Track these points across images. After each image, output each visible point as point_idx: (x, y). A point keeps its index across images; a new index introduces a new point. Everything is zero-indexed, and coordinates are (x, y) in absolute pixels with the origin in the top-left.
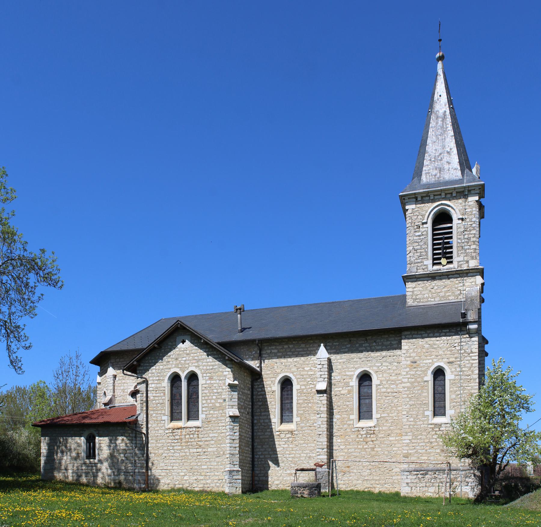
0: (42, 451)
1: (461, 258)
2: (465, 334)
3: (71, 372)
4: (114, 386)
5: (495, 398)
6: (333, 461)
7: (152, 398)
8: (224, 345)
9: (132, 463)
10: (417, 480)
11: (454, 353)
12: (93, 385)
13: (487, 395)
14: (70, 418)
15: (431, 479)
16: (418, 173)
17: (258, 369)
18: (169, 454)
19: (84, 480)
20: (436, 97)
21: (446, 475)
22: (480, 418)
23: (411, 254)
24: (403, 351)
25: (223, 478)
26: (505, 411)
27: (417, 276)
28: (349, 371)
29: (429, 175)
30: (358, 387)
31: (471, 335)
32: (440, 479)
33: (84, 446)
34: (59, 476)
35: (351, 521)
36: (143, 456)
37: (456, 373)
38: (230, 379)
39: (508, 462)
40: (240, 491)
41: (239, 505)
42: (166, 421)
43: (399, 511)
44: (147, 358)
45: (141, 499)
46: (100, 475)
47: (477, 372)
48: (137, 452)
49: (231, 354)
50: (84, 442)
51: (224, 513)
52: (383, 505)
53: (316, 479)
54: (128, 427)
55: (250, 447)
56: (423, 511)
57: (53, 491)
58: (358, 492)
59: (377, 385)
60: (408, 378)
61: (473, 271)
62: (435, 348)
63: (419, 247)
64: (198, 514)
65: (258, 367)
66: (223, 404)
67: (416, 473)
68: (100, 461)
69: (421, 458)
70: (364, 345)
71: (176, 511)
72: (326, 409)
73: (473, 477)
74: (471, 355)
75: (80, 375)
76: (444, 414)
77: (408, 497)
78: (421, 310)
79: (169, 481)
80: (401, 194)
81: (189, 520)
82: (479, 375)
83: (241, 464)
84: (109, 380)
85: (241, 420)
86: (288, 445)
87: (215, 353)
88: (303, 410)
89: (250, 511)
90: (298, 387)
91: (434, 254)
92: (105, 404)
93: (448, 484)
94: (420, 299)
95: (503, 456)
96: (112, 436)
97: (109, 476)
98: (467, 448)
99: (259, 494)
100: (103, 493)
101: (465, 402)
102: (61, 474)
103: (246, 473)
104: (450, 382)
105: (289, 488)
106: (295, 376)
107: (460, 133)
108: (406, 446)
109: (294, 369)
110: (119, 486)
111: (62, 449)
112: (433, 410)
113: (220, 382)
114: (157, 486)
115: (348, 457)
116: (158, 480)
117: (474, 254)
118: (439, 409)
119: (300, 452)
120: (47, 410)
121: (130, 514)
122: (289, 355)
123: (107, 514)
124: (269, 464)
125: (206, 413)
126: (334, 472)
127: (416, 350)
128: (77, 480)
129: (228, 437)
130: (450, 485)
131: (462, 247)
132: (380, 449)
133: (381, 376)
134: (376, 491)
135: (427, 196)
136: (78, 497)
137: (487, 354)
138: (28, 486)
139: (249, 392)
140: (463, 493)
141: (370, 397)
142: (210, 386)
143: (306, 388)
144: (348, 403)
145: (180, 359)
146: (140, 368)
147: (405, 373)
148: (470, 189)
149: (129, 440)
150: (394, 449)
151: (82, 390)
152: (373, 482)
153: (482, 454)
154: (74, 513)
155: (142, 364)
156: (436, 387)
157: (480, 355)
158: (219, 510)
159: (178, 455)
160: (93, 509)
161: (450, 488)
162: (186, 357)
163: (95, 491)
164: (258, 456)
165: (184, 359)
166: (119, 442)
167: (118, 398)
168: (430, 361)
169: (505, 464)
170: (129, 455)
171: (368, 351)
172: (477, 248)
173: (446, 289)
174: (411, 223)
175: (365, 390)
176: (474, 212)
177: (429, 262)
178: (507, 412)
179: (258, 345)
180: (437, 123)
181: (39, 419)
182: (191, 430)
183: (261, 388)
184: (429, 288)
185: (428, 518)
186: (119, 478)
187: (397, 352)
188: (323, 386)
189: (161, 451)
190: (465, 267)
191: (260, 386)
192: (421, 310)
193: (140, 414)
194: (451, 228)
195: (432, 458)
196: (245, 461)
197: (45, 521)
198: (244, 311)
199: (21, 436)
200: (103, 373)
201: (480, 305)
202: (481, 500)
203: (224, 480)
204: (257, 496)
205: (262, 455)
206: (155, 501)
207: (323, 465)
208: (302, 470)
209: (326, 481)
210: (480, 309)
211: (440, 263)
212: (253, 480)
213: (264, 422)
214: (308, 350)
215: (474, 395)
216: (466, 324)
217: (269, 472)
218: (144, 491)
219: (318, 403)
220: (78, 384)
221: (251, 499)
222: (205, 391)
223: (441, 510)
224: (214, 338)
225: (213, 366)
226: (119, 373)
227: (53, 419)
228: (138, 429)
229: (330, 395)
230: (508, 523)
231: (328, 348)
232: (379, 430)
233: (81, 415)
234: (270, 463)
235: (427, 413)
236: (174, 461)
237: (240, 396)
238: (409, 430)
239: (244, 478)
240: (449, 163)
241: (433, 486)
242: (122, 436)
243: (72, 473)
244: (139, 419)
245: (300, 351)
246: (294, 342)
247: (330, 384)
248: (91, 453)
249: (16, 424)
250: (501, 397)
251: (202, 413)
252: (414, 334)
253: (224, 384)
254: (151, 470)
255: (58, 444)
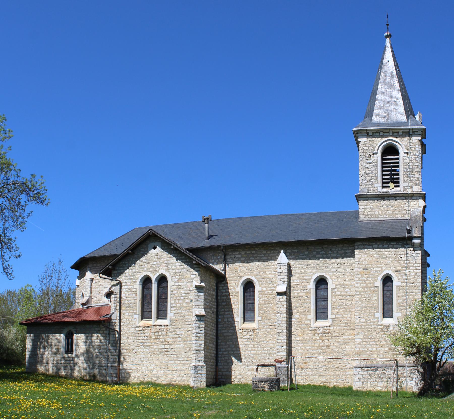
0: (27, 347)
1: (406, 184)
2: (410, 247)
3: (54, 276)
4: (91, 288)
5: (436, 303)
6: (291, 357)
7: (125, 298)
8: (193, 251)
9: (105, 358)
10: (368, 376)
11: (401, 263)
12: (72, 288)
13: (428, 301)
14: (51, 317)
15: (381, 375)
16: (370, 114)
17: (223, 272)
18: (139, 350)
19: (62, 372)
20: (385, 62)
21: (393, 371)
22: (423, 321)
23: (363, 178)
24: (356, 259)
25: (188, 372)
26: (444, 315)
27: (368, 196)
28: (307, 276)
29: (379, 116)
30: (315, 290)
31: (415, 249)
32: (388, 375)
33: (63, 342)
34: (41, 369)
35: (308, 413)
36: (116, 352)
37: (402, 280)
38: (197, 282)
39: (447, 360)
40: (205, 385)
41: (204, 398)
42: (137, 319)
43: (352, 403)
44: (121, 263)
45: (113, 391)
46: (77, 368)
47: (420, 280)
48: (110, 348)
49: (198, 259)
50: (63, 338)
51: (189, 405)
52: (337, 398)
53: (276, 374)
54: (102, 325)
55: (215, 343)
56: (373, 404)
57: (36, 382)
58: (314, 386)
59: (332, 289)
60: (361, 283)
61: (417, 195)
62: (384, 258)
63: (370, 172)
64: (165, 405)
65: (223, 270)
66: (190, 304)
67: (367, 369)
68: (77, 356)
69: (371, 355)
70: (320, 253)
71: (144, 402)
72: (285, 309)
73: (417, 373)
74: (415, 265)
75: (61, 279)
76: (392, 317)
77: (360, 391)
78: (372, 225)
79: (139, 375)
80: (354, 129)
81: (156, 411)
82: (422, 283)
83: (206, 360)
84: (86, 283)
85: (206, 319)
86: (250, 342)
87: (183, 257)
88: (264, 310)
89: (213, 404)
90: (260, 289)
91: (383, 179)
92: (83, 305)
93: (395, 379)
94: (371, 215)
95: (443, 355)
96: (88, 333)
97: (85, 369)
98: (412, 347)
99: (222, 388)
100: (79, 385)
101: (410, 306)
102: (42, 367)
103: (211, 368)
104: (397, 288)
105: (250, 383)
106: (257, 279)
107: (405, 89)
108: (359, 344)
109: (257, 273)
110: (93, 379)
111: (44, 345)
112: (382, 312)
113: (188, 284)
114: (127, 379)
115: (306, 354)
116: (129, 373)
117: (417, 182)
118: (387, 312)
119: (261, 349)
120: (32, 310)
121: (102, 404)
122: (251, 260)
123: (82, 404)
124: (232, 360)
125: (174, 312)
126: (293, 368)
127: (367, 259)
128: (57, 373)
129: (194, 335)
130: (397, 380)
131: (407, 175)
132: (335, 347)
133: (336, 280)
134: (331, 385)
135: (377, 132)
136: (57, 388)
137: (428, 266)
138: (15, 378)
139: (214, 293)
140: (408, 388)
141: (326, 299)
142: (179, 287)
143: (267, 290)
144: (306, 305)
145: (151, 264)
146: (115, 272)
147: (357, 279)
148: (414, 130)
149: (103, 336)
150: (347, 347)
151: (63, 292)
152: (328, 377)
153: (425, 353)
154: (53, 403)
155: (117, 268)
156: (385, 292)
157: (423, 266)
158: (185, 402)
159: (148, 351)
160: (69, 399)
161: (397, 383)
162: (157, 262)
163: (71, 383)
164: (222, 353)
165: (155, 263)
166: (94, 338)
167: (94, 299)
168: (380, 269)
169: (444, 361)
170: (103, 350)
171: (324, 258)
172: (420, 177)
173: (393, 208)
174: (363, 153)
175: (321, 293)
176: (417, 149)
177: (379, 185)
178: (445, 316)
179: (223, 250)
180: (385, 80)
181: (25, 318)
182: (160, 328)
183: (225, 289)
184: (379, 207)
185: (378, 410)
186: (94, 371)
187: (351, 260)
188: (283, 288)
189: (132, 347)
190: (410, 191)
191: (225, 288)
192: (372, 225)
193: (113, 313)
194: (398, 159)
195: (381, 356)
196: (209, 357)
197: (27, 409)
198: (211, 221)
199: (10, 333)
200: (81, 277)
201: (423, 224)
202: (424, 394)
203: (189, 375)
204: (221, 389)
205: (225, 351)
206: (125, 393)
207: (283, 361)
208: (263, 365)
209: (285, 376)
210: (422, 227)
211: (389, 187)
212: (216, 375)
213: (228, 321)
214: (269, 256)
215: (418, 300)
216: (411, 238)
217: (233, 367)
218: (116, 383)
219: (278, 304)
220: (60, 287)
221: (214, 392)
222: (173, 292)
223: (389, 403)
224: (182, 244)
225: (181, 269)
226: (96, 276)
227: (37, 318)
228: (111, 327)
229: (290, 296)
230: (447, 413)
231: (288, 254)
232: (334, 330)
233: (60, 314)
234: (233, 359)
235: (377, 315)
236: (143, 356)
237: (206, 297)
238: (361, 330)
239: (208, 372)
240: (396, 110)
241: (382, 381)
242: (97, 333)
243: (52, 366)
244: (113, 317)
245: (262, 257)
246: (256, 249)
247: (289, 287)
248: (69, 349)
249: (6, 323)
250: (440, 302)
251: (171, 313)
252: (366, 245)
253: (192, 285)
254: (122, 364)
255: (41, 340)
